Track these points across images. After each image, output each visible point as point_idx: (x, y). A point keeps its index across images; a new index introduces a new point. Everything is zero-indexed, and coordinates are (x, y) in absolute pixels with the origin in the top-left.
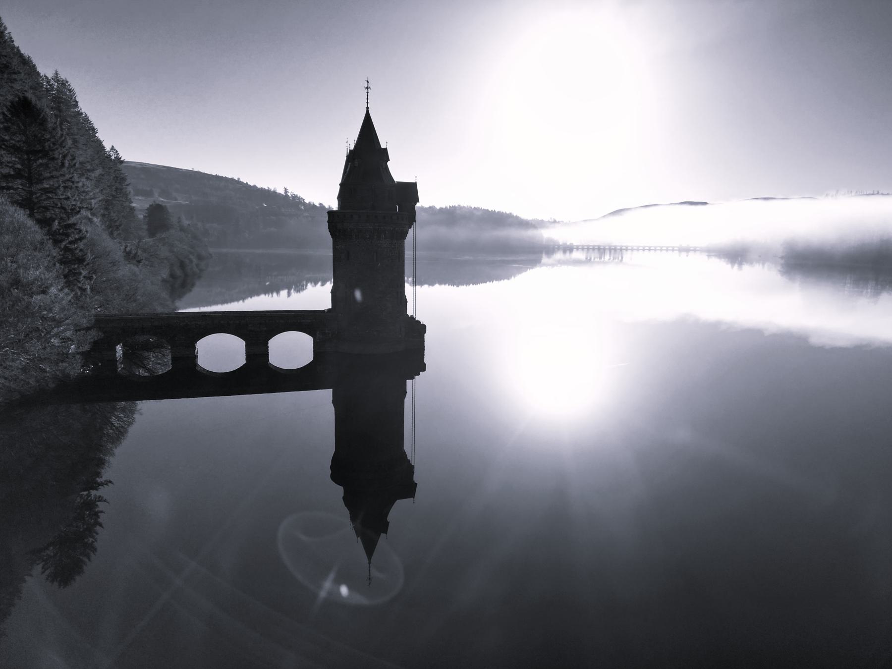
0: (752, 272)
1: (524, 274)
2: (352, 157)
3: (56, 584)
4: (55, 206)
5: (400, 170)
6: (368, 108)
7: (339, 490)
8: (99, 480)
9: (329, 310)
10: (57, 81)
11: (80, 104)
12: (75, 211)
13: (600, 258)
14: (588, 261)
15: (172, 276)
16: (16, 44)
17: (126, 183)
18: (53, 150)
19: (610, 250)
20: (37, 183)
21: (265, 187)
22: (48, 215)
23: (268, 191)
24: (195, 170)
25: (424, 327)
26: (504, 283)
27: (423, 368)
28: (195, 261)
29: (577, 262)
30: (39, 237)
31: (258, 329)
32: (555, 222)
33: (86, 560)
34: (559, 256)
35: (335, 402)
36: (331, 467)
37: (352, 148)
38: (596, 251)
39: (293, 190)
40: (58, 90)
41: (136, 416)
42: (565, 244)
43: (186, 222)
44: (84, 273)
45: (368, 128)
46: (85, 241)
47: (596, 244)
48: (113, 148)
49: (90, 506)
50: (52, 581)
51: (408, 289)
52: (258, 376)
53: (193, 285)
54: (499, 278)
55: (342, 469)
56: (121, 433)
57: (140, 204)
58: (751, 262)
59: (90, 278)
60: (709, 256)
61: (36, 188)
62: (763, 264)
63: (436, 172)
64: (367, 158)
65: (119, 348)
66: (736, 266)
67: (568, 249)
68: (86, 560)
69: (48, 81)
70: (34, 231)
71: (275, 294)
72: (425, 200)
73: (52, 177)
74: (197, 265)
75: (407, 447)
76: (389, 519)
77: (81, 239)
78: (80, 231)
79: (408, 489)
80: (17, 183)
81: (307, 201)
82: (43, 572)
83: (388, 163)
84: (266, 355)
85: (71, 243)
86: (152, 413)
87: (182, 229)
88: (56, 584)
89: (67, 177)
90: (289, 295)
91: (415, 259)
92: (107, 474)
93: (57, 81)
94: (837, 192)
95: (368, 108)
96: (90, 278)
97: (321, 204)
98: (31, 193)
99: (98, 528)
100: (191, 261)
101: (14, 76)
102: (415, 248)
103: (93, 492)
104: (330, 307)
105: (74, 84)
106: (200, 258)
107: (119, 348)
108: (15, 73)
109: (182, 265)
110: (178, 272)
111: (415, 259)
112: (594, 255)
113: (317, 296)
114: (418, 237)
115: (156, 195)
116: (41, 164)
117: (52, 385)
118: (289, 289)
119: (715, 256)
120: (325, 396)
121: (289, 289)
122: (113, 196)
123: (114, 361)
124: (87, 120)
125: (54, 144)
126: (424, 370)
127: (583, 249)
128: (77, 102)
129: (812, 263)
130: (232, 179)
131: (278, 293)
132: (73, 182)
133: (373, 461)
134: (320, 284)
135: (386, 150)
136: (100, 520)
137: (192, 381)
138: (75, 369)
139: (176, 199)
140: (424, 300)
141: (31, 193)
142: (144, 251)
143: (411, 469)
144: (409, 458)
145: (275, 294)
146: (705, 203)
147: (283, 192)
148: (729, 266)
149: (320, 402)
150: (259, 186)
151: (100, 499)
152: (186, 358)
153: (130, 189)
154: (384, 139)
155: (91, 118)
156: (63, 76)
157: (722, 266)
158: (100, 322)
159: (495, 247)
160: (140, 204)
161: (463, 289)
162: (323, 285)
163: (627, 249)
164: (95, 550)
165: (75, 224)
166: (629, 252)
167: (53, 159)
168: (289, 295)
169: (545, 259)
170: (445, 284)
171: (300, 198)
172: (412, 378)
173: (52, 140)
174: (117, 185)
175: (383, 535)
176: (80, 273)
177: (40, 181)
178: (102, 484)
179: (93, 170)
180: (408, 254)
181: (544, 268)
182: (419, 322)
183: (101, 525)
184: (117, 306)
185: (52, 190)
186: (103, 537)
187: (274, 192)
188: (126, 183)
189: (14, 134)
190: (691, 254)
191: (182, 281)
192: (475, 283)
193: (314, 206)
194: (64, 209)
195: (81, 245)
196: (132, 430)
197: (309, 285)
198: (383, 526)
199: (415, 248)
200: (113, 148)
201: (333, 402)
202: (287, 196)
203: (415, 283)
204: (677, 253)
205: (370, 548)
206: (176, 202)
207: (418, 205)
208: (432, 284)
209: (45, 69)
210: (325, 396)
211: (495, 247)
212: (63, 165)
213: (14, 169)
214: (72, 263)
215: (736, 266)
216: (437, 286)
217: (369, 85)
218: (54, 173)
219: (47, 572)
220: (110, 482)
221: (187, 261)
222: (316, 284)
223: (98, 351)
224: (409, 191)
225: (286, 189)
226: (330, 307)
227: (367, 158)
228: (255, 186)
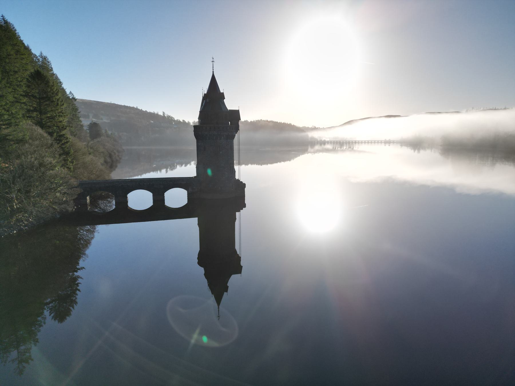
0: (426, 154)
1: (298, 158)
2: (205, 97)
3: (57, 321)
4: (54, 125)
5: (230, 104)
7: (202, 270)
8: (78, 267)
9: (195, 177)
10: (42, 57)
11: (53, 69)
13: (341, 148)
14: (334, 150)
15: (106, 162)
16: (22, 39)
17: (79, 111)
18: (52, 97)
19: (346, 143)
20: (45, 114)
21: (152, 111)
22: (51, 131)
23: (154, 114)
24: (112, 103)
25: (245, 184)
27: (244, 206)
28: (117, 154)
29: (328, 151)
30: (50, 142)
31: (159, 187)
33: (71, 308)
34: (317, 147)
35: (199, 224)
36: (198, 258)
37: (206, 93)
38: (348, 144)
39: (168, 113)
40: (43, 62)
41: (96, 234)
43: (110, 133)
44: (70, 160)
45: (213, 83)
46: (69, 143)
47: (380, 140)
48: (71, 93)
49: (75, 279)
50: (55, 320)
51: (236, 167)
52: (159, 212)
53: (116, 166)
54: (284, 160)
55: (202, 260)
56: (87, 243)
57: (86, 122)
58: (424, 148)
59: (72, 162)
60: (401, 146)
61: (44, 116)
62: (431, 150)
63: (249, 106)
64: (213, 98)
65: (88, 198)
66: (416, 151)
67: (324, 143)
68: (71, 308)
69: (37, 57)
70: (49, 140)
71: (159, 172)
72: (243, 118)
73: (52, 110)
74: (118, 156)
75: (237, 247)
76: (228, 285)
77: (67, 142)
78: (67, 138)
79: (238, 269)
80: (35, 114)
81: (176, 119)
82: (50, 315)
83: (225, 100)
84: (163, 200)
85: (63, 144)
86: (104, 232)
87: (108, 136)
88: (57, 321)
89: (60, 111)
90: (167, 172)
91: (239, 150)
92: (82, 263)
93: (42, 57)
94: (473, 108)
96: (72, 162)
97: (184, 121)
98: (42, 119)
99: (78, 292)
100: (115, 154)
101: (23, 56)
102: (239, 144)
103: (75, 273)
104: (195, 175)
105: (50, 59)
106: (118, 151)
107: (88, 198)
108: (22, 55)
109: (110, 156)
110: (109, 160)
111: (239, 150)
112: (337, 147)
113: (189, 170)
114: (241, 138)
115: (91, 117)
116: (46, 104)
117: (58, 216)
118: (167, 168)
119: (405, 145)
120: (194, 221)
121: (167, 168)
122: (72, 119)
123: (86, 204)
124: (57, 78)
125: (53, 94)
127: (331, 143)
128: (52, 68)
129: (456, 148)
130: (133, 108)
131: (160, 171)
132: (63, 113)
133: (219, 259)
134: (184, 165)
135: (223, 93)
136: (78, 288)
137: (125, 215)
138: (71, 208)
139: (102, 119)
140: (243, 172)
141: (42, 119)
142: (91, 148)
143: (239, 258)
144: (238, 253)
145: (159, 172)
146: (399, 116)
147: (162, 114)
148: (413, 151)
149: (191, 225)
150: (148, 111)
151: (79, 277)
152: (123, 202)
153: (79, 115)
155: (59, 76)
156: (44, 54)
157: (408, 151)
158: (82, 185)
159: (285, 142)
160: (86, 122)
161: (264, 167)
162: (185, 166)
163: (355, 143)
164: (76, 303)
165: (64, 135)
166: (357, 144)
167: (53, 101)
168: (167, 172)
169: (310, 149)
170: (254, 164)
171: (172, 117)
172: (239, 211)
173: (52, 91)
174: (74, 113)
175: (225, 293)
176: (68, 160)
177: (45, 113)
178: (79, 269)
180: (236, 147)
181: (310, 154)
182: (242, 182)
183: (79, 290)
184: (85, 177)
185: (52, 118)
186: (80, 297)
187: (157, 114)
188: (79, 111)
189: (33, 89)
190: (391, 144)
191: (112, 163)
192: (272, 163)
193: (180, 121)
194: (59, 127)
195: (68, 145)
196: (93, 242)
197: (178, 166)
198: (226, 289)
199: (239, 144)
200: (71, 93)
201: (198, 224)
202: (164, 116)
203: (239, 164)
204: (383, 144)
205: (218, 299)
206: (104, 120)
208: (247, 164)
209: (36, 51)
210: (194, 221)
211: (285, 142)
213: (33, 107)
214: (66, 154)
215: (416, 151)
216: (250, 165)
218: (53, 109)
219: (52, 315)
220: (84, 268)
221: (113, 154)
222: (182, 166)
223: (79, 200)
224: (236, 114)
225: (164, 113)
226: (195, 175)
227: (213, 98)
228: (146, 111)
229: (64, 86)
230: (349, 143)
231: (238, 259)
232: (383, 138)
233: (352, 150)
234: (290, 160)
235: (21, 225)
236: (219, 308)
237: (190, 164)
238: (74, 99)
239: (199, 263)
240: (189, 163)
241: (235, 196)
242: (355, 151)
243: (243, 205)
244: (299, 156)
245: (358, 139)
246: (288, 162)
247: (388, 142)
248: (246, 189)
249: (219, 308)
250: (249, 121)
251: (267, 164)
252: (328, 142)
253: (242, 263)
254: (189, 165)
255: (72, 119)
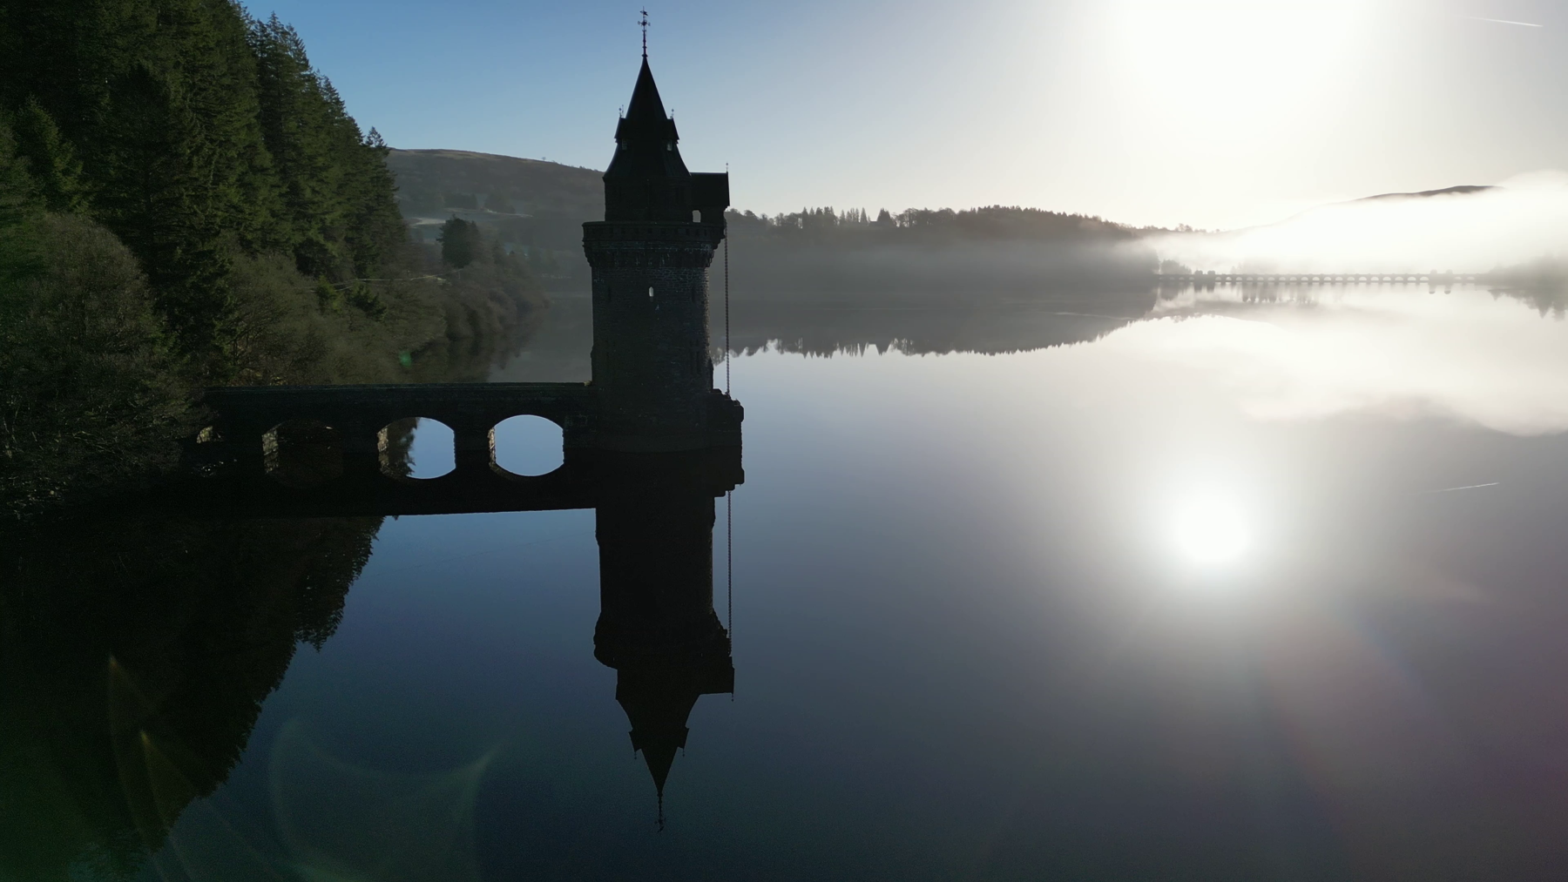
5: (697, 154)
6: (645, 56)
10: (275, 29)
12: (209, 232)
19: (1288, 283)
26: (1081, 348)
27: (739, 477)
32: (1189, 229)
34: (1188, 296)
42: (1199, 273)
44: (219, 325)
45: (646, 89)
48: (373, 132)
52: (478, 485)
55: (608, 643)
57: (428, 223)
63: (774, 162)
66: (1551, 312)
67: (1207, 282)
72: (740, 201)
79: (721, 678)
93: (275, 29)
95: (645, 56)
97: (749, 213)
104: (586, 378)
110: (464, 329)
120: (584, 520)
122: (368, 207)
126: (742, 481)
127: (1233, 283)
133: (663, 625)
134: (745, 351)
140: (753, 375)
148: (1536, 311)
154: (672, 104)
156: (284, 21)
157: (1516, 311)
160: (428, 223)
162: (750, 354)
165: (211, 252)
170: (968, 349)
176: (214, 326)
179: (325, 168)
195: (220, 282)
198: (680, 736)
200: (373, 132)
204: (1425, 287)
207: (728, 209)
210: (584, 520)
212: (190, 165)
216: (953, 353)
217: (648, 19)
229: (350, 110)
230: (1266, 284)
231: (721, 641)
232: (1425, 269)
233: (1308, 307)
234: (1090, 340)
235: (17, 507)
236: (660, 795)
237: (765, 349)
238: (383, 150)
239: (598, 654)
240: (763, 344)
241: (712, 440)
242: (1282, 305)
243: (735, 476)
244: (1123, 324)
245: (1316, 270)
246: (1085, 343)
247: (1442, 282)
248: (746, 426)
249: (660, 795)
250: (957, 211)
251: (1011, 349)
252: (1223, 280)
253: (736, 654)
254: (760, 351)
255: (370, 209)
